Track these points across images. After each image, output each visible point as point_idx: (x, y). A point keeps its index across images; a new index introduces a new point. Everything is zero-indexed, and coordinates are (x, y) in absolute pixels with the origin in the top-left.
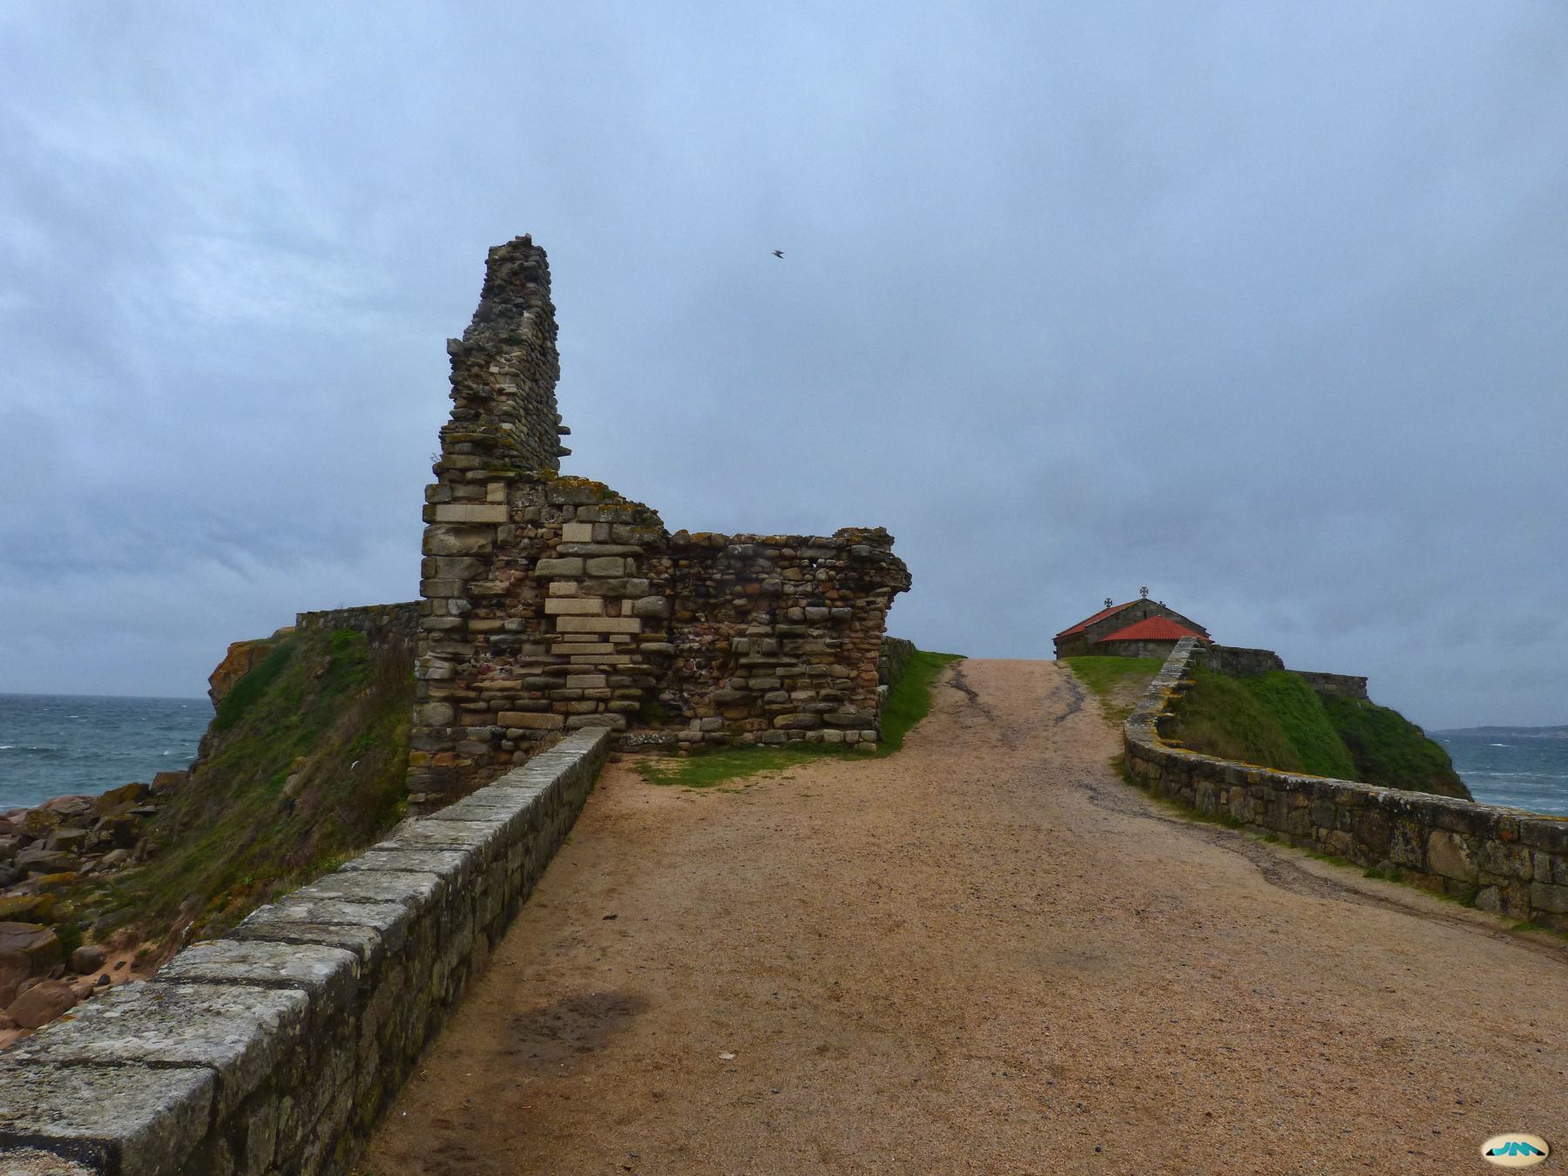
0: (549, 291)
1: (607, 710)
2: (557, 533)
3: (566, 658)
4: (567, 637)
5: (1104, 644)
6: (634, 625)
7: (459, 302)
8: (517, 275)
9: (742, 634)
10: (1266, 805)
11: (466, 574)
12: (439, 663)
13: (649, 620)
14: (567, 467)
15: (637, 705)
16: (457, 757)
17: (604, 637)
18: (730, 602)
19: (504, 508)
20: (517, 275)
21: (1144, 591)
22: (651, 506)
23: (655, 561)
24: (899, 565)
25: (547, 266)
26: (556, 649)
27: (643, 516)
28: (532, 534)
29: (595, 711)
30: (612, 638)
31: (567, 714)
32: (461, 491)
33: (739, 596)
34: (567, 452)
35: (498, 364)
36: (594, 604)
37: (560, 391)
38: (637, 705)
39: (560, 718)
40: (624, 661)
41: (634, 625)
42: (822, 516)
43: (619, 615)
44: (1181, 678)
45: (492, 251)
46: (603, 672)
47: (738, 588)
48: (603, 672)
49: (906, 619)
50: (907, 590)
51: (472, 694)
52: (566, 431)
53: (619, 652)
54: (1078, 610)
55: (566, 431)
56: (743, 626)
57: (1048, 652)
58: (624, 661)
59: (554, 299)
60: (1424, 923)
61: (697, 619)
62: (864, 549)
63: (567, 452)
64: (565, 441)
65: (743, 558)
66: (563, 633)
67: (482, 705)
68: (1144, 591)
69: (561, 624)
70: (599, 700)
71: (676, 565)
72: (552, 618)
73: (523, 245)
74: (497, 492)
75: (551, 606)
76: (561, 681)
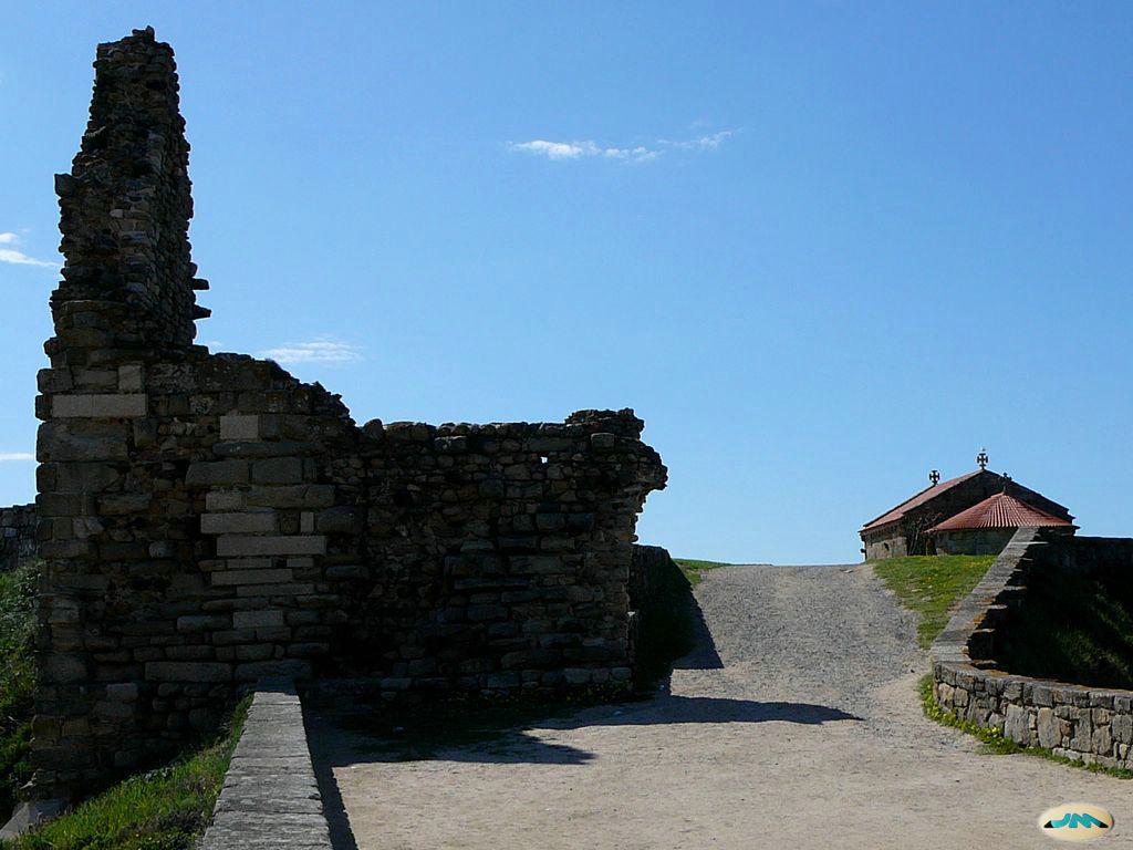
0: (176, 100)
1: (286, 656)
2: (213, 430)
3: (231, 591)
4: (231, 563)
5: (932, 528)
6: (317, 545)
7: (61, 126)
8: (136, 95)
9: (454, 551)
10: (1072, 727)
11: (95, 488)
12: (63, 604)
13: (335, 538)
14: (212, 336)
15: (325, 647)
16: (95, 721)
17: (281, 562)
18: (440, 510)
19: (141, 399)
20: (136, 95)
21: (983, 459)
22: (331, 388)
23: (340, 462)
24: (652, 458)
25: (174, 66)
26: (217, 579)
27: (321, 404)
28: (179, 430)
29: (272, 657)
30: (289, 563)
31: (235, 662)
32: (87, 377)
33: (451, 504)
34: (205, 313)
35: (123, 206)
36: (266, 521)
37: (196, 232)
38: (325, 647)
39: (227, 667)
40: (306, 591)
41: (317, 545)
42: (543, 399)
43: (297, 533)
44: (1009, 583)
45: (103, 49)
46: (280, 605)
47: (449, 494)
48: (280, 605)
49: (659, 524)
50: (662, 487)
51: (112, 643)
52: (203, 285)
53: (297, 579)
54: (903, 488)
55: (203, 285)
56: (456, 541)
57: (850, 551)
58: (306, 591)
59: (184, 110)
60: (222, 583)
61: (398, 534)
62: (607, 438)
63: (205, 313)
64: (201, 299)
65: (453, 452)
66: (225, 558)
67: (122, 656)
68: (983, 459)
69: (223, 548)
70: (276, 642)
71: (367, 464)
72: (211, 539)
73: (143, 40)
74: (131, 375)
75: (209, 524)
76: (225, 620)
